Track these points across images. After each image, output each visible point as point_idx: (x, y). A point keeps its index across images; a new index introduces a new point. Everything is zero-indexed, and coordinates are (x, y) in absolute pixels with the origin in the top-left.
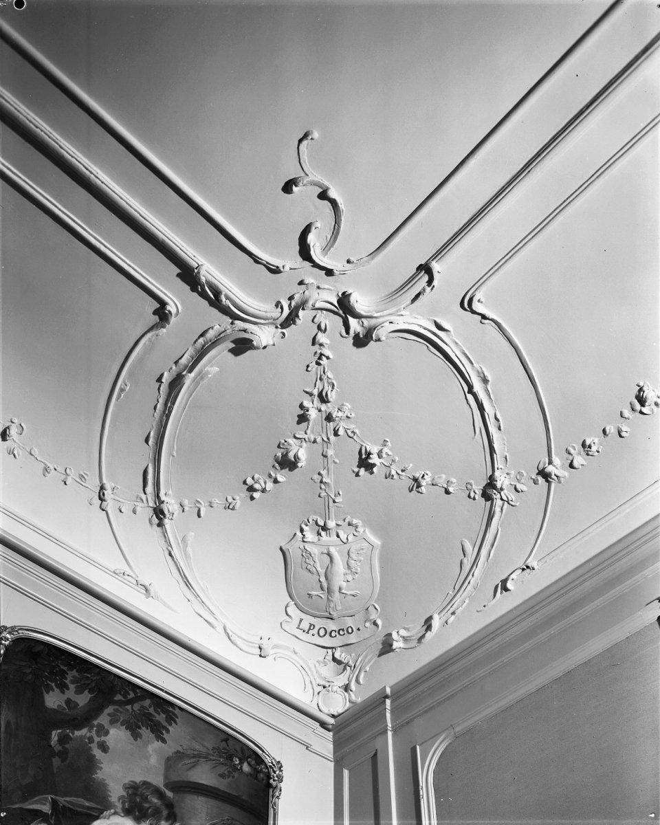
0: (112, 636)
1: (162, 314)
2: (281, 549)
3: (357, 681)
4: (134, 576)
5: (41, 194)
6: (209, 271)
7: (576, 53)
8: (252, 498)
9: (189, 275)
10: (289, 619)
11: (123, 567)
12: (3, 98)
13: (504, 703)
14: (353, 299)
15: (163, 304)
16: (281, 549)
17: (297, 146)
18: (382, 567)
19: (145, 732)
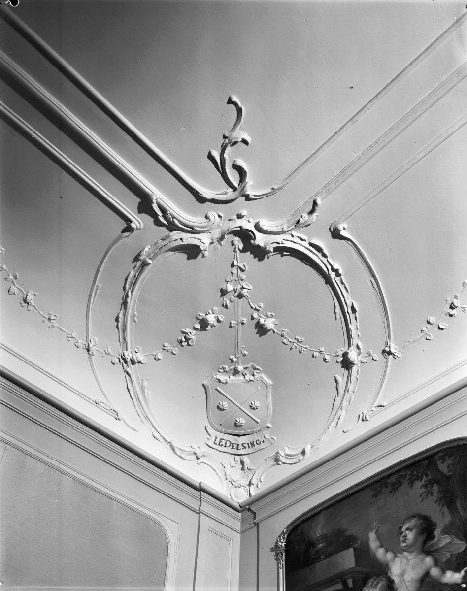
0: (71, 438)
1: (128, 229)
2: (203, 385)
3: (261, 481)
4: (107, 403)
5: (33, 131)
6: (158, 195)
7: (401, 417)
8: (182, 346)
9: (145, 204)
10: (209, 437)
11: (99, 398)
12: (3, 59)
13: (272, 410)
14: (260, 224)
15: (128, 221)
16: (203, 385)
17: (275, 241)
18: (273, 402)
19: (425, 534)
